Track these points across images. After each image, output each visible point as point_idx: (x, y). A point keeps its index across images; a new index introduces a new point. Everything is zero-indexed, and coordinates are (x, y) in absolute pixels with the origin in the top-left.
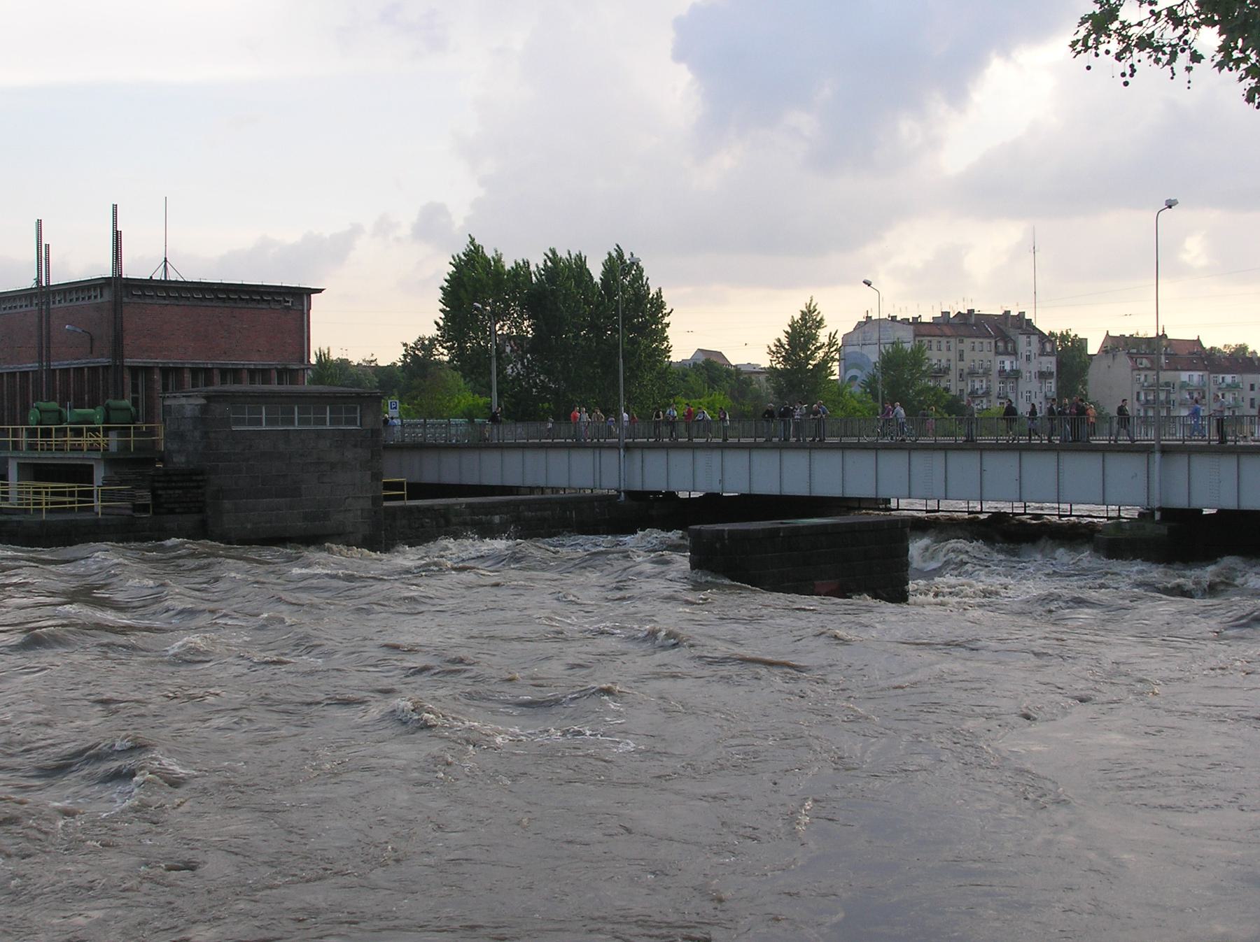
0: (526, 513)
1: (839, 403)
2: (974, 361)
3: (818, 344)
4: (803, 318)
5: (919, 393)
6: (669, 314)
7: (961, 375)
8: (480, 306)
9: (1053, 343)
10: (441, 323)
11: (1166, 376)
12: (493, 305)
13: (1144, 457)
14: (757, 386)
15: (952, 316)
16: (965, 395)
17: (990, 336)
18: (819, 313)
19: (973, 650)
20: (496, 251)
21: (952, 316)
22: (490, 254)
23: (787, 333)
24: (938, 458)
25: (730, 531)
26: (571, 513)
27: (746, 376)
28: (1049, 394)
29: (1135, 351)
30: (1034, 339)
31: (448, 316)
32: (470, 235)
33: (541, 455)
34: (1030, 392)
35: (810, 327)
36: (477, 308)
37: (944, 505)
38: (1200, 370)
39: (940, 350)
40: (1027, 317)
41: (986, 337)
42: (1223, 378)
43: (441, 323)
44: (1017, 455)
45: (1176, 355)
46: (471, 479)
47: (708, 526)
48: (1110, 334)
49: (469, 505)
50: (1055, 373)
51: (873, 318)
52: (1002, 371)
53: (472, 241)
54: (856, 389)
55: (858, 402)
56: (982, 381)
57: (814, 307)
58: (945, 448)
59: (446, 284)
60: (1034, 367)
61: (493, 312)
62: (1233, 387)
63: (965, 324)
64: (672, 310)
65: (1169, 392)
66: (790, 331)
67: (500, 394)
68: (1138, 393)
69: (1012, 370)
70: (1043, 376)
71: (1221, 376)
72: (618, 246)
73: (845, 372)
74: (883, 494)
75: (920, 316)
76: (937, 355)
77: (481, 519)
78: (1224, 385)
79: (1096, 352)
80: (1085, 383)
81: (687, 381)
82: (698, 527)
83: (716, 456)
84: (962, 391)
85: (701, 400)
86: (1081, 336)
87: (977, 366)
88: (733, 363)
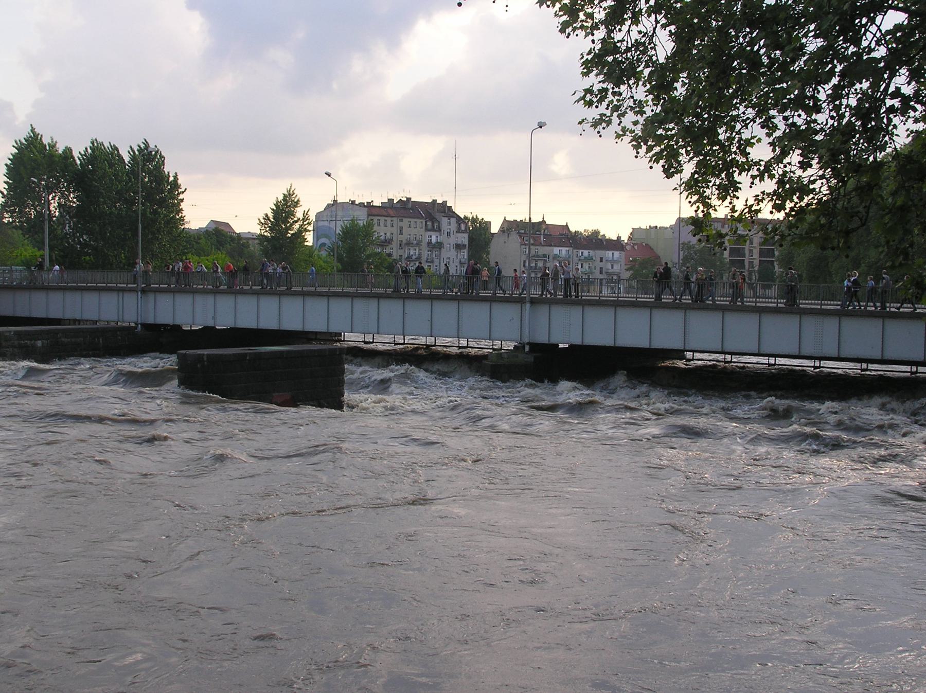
0: (63, 339)
1: (310, 262)
2: (410, 235)
3: (296, 219)
4: (284, 199)
5: (369, 256)
6: (183, 192)
7: (400, 245)
8: (36, 180)
9: (466, 224)
10: (5, 192)
11: (542, 250)
12: (47, 181)
13: (517, 307)
14: (252, 249)
15: (395, 202)
16: (403, 260)
17: (422, 218)
18: (296, 196)
19: (249, 440)
20: (52, 139)
21: (395, 202)
22: (46, 141)
23: (273, 209)
24: (373, 303)
25: (208, 355)
26: (98, 339)
27: (244, 241)
28: (463, 260)
29: (523, 231)
30: (453, 220)
31: (11, 187)
32: (31, 125)
33: (77, 296)
34: (449, 258)
35: (290, 206)
36: (34, 182)
37: (378, 338)
38: (567, 247)
39: (386, 226)
40: (448, 205)
41: (418, 218)
42: (582, 253)
43: (5, 192)
44: (613, 310)
45: (550, 235)
46: (21, 312)
47: (192, 351)
48: (507, 219)
49: (16, 333)
50: (467, 246)
51: (338, 202)
52: (430, 243)
53: (33, 130)
54: (324, 254)
55: (324, 262)
56: (415, 250)
57: (293, 191)
58: (379, 297)
59: (9, 162)
60: (453, 240)
61: (47, 186)
62: (589, 259)
63: (405, 208)
64: (186, 189)
65: (545, 261)
66: (275, 209)
67: (51, 248)
68: (525, 262)
69: (437, 242)
70: (459, 247)
71: (581, 251)
72: (145, 140)
73: (318, 240)
74: (333, 329)
75: (372, 201)
76: (382, 230)
77: (26, 343)
78: (582, 258)
79: (497, 232)
80: (488, 253)
81: (199, 243)
82: (184, 352)
83: (210, 299)
84: (401, 256)
85: (208, 258)
86: (486, 219)
87: (412, 238)
88: (238, 232)
